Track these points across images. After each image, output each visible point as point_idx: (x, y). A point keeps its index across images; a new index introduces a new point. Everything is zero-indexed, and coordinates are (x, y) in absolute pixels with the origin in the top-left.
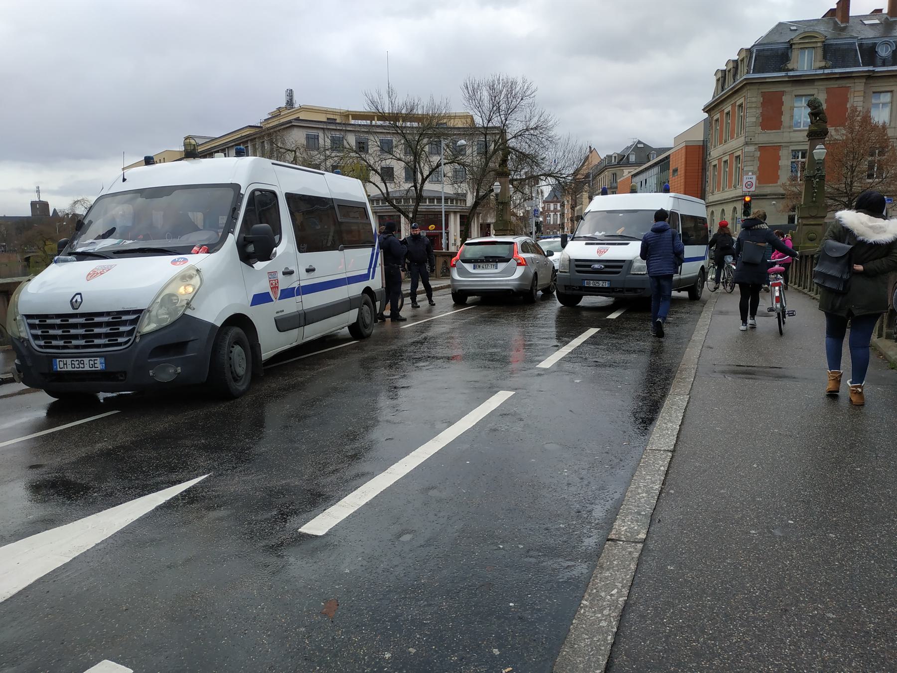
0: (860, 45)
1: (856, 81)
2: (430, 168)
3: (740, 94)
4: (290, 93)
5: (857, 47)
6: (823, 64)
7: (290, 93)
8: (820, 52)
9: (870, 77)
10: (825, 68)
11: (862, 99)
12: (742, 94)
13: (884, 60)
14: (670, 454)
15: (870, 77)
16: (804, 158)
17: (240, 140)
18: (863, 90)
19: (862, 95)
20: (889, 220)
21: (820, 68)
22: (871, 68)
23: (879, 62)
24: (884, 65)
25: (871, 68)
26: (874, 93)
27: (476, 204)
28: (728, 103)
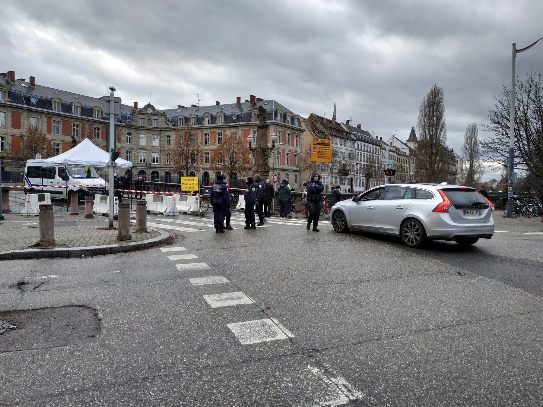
1: (24, 111)
6: (9, 100)
8: (7, 94)
9: (30, 111)
10: (10, 102)
15: (30, 111)
21: (8, 101)
22: (30, 107)
24: (34, 106)
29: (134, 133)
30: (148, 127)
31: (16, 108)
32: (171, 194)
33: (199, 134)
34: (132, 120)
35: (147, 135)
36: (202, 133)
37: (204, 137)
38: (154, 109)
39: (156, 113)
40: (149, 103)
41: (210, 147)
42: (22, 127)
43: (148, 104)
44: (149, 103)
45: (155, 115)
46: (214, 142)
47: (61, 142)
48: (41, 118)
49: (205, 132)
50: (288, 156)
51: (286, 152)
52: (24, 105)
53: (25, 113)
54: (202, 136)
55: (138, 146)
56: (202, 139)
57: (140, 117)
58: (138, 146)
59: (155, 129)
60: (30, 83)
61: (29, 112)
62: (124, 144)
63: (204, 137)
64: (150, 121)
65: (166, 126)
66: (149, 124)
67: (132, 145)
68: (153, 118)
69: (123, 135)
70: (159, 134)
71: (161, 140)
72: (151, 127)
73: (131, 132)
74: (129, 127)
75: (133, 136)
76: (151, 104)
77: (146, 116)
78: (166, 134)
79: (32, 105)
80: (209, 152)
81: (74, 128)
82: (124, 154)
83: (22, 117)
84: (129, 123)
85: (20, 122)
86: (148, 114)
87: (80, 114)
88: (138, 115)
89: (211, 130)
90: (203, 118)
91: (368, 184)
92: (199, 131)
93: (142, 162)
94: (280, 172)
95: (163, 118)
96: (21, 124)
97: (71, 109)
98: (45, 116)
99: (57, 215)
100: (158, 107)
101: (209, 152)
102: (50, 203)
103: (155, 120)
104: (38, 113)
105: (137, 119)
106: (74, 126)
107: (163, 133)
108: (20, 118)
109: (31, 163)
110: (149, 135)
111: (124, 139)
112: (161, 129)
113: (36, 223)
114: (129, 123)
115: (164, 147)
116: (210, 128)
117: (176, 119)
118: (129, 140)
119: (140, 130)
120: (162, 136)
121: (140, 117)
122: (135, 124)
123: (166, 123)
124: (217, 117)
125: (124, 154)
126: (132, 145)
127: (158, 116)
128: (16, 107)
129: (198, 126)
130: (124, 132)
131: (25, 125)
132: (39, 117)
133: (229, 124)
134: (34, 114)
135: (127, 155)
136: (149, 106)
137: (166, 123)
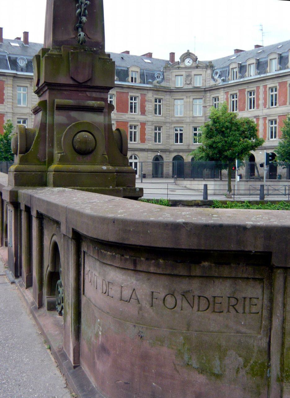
0: (9, 58)
1: (8, 78)
2: (249, 156)
3: (199, 93)
4: (26, 34)
5: (8, 59)
7: (26, 34)
9: (15, 77)
11: (11, 89)
12: (164, 94)
13: (22, 68)
14: (265, 192)
16: (135, 129)
17: (164, 89)
18: (12, 83)
19: (12, 86)
20: (197, 57)
22: (14, 72)
23: (20, 69)
24: (22, 70)
25: (14, 72)
26: (18, 86)
27: (85, 11)
28: (269, 82)
29: (166, 98)
30: (186, 87)
32: (99, 250)
33: (261, 90)
34: (163, 79)
35: (185, 100)
36: (265, 87)
37: (269, 93)
38: (195, 60)
40: (188, 51)
41: (278, 109)
42: (6, 100)
43: (186, 51)
44: (188, 51)
45: (197, 67)
46: (284, 101)
47: (139, 124)
49: (270, 84)
51: (129, 124)
52: (9, 69)
53: (9, 82)
54: (265, 92)
55: (173, 119)
56: (265, 99)
57: (174, 74)
58: (173, 119)
59: (196, 90)
60: (23, 42)
61: (16, 79)
62: (151, 116)
63: (269, 93)
64: (190, 78)
65: (212, 83)
66: (188, 83)
67: (162, 116)
69: (149, 103)
71: (206, 107)
72: (190, 87)
74: (156, 90)
75: (164, 102)
76: (190, 51)
77: (184, 70)
78: (213, 96)
79: (20, 69)
80: (277, 118)
81: (132, 101)
82: (150, 132)
83: (5, 86)
84: (158, 85)
85: (3, 94)
86: (186, 68)
88: (172, 71)
89: (280, 80)
90: (266, 63)
91: (121, 88)
92: (261, 85)
95: (209, 71)
100: (203, 57)
101: (277, 118)
104: (26, 80)
105: (170, 77)
106: (131, 99)
107: (208, 94)
108: (3, 89)
110: (188, 100)
111: (151, 109)
112: (205, 89)
113: (208, 189)
114: (158, 85)
116: (278, 77)
117: (227, 70)
118: (157, 110)
119: (174, 93)
121: (174, 74)
123: (213, 78)
125: (150, 132)
126: (162, 116)
127: (201, 70)
129: (259, 76)
130: (151, 99)
131: (9, 97)
132: (28, 85)
134: (22, 82)
135: (156, 134)
136: (188, 55)
137: (213, 78)
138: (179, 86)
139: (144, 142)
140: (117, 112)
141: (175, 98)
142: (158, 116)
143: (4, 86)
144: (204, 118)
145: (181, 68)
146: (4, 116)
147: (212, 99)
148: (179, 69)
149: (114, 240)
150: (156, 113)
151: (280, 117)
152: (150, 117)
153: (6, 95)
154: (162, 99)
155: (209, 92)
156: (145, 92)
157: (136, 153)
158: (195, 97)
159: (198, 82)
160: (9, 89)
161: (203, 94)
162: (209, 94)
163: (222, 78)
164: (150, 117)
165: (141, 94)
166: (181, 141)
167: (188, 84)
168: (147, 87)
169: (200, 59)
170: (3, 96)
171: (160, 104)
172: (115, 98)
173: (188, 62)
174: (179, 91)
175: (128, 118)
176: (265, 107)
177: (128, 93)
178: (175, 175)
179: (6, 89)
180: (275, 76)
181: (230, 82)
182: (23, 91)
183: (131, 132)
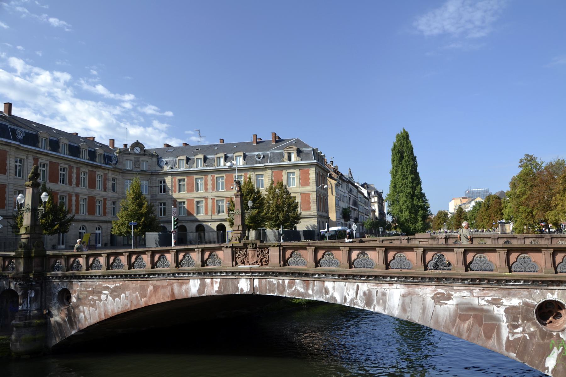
31: (4, 144)
39: (145, 153)
40: (137, 141)
42: (8, 171)
44: (137, 141)
45: (145, 155)
47: (102, 199)
48: (28, 159)
50: (114, 205)
52: (10, 139)
64: (138, 163)
66: (137, 166)
68: (142, 158)
70: (148, 179)
71: (152, 187)
72: (138, 170)
73: (116, 177)
74: (115, 170)
76: (139, 142)
78: (158, 179)
83: (8, 157)
85: (6, 165)
86: (135, 154)
87: (68, 154)
93: (163, 216)
94: (85, 224)
96: (7, 167)
97: (59, 147)
98: (33, 156)
99: (476, 291)
102: (150, 286)
103: (144, 161)
104: (24, 152)
107: (154, 177)
108: (6, 159)
109: (58, 225)
115: (156, 195)
117: (173, 160)
120: (153, 181)
121: (125, 158)
122: (120, 167)
124: (235, 157)
127: (147, 157)
128: (4, 143)
133: (253, 166)
138: (128, 168)
139: (105, 215)
140: (89, 188)
141: (125, 178)
142: (17, 179)
143: (7, 157)
144: (150, 196)
145: (131, 154)
146: (6, 187)
147: (158, 181)
148: (129, 154)
149: (129, 304)
150: (16, 175)
151: (227, 198)
152: (110, 194)
153: (8, 165)
154: (116, 178)
155: (155, 175)
156: (106, 172)
157: (101, 224)
158: (142, 179)
159: (145, 167)
160: (11, 159)
161: (149, 177)
162: (155, 177)
163: (170, 166)
164: (110, 194)
165: (104, 173)
166: (164, 214)
167: (137, 168)
168: (109, 168)
169: (146, 148)
170: (6, 167)
171: (64, 173)
172: (87, 175)
173: (137, 150)
174: (130, 172)
175: (96, 194)
176: (213, 190)
177: (96, 171)
178: (344, 242)
179: (9, 160)
180: (57, 157)
181: (179, 170)
182: (261, 178)
183: (161, 209)
